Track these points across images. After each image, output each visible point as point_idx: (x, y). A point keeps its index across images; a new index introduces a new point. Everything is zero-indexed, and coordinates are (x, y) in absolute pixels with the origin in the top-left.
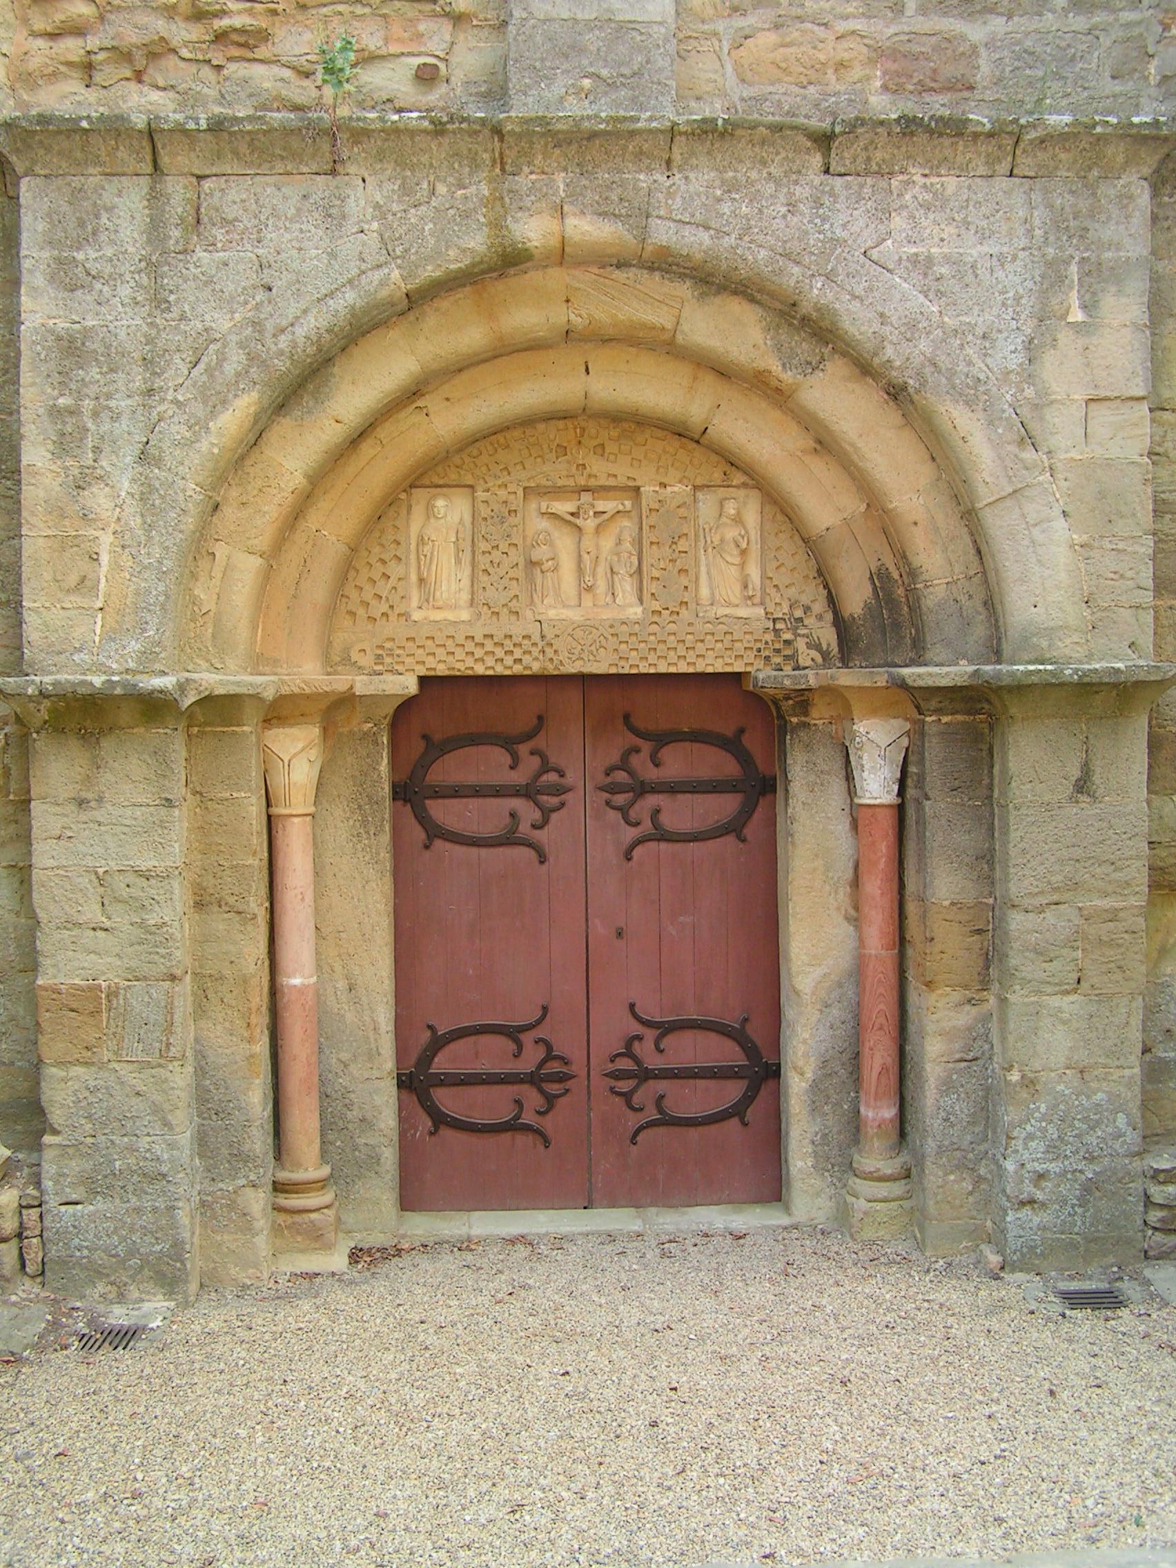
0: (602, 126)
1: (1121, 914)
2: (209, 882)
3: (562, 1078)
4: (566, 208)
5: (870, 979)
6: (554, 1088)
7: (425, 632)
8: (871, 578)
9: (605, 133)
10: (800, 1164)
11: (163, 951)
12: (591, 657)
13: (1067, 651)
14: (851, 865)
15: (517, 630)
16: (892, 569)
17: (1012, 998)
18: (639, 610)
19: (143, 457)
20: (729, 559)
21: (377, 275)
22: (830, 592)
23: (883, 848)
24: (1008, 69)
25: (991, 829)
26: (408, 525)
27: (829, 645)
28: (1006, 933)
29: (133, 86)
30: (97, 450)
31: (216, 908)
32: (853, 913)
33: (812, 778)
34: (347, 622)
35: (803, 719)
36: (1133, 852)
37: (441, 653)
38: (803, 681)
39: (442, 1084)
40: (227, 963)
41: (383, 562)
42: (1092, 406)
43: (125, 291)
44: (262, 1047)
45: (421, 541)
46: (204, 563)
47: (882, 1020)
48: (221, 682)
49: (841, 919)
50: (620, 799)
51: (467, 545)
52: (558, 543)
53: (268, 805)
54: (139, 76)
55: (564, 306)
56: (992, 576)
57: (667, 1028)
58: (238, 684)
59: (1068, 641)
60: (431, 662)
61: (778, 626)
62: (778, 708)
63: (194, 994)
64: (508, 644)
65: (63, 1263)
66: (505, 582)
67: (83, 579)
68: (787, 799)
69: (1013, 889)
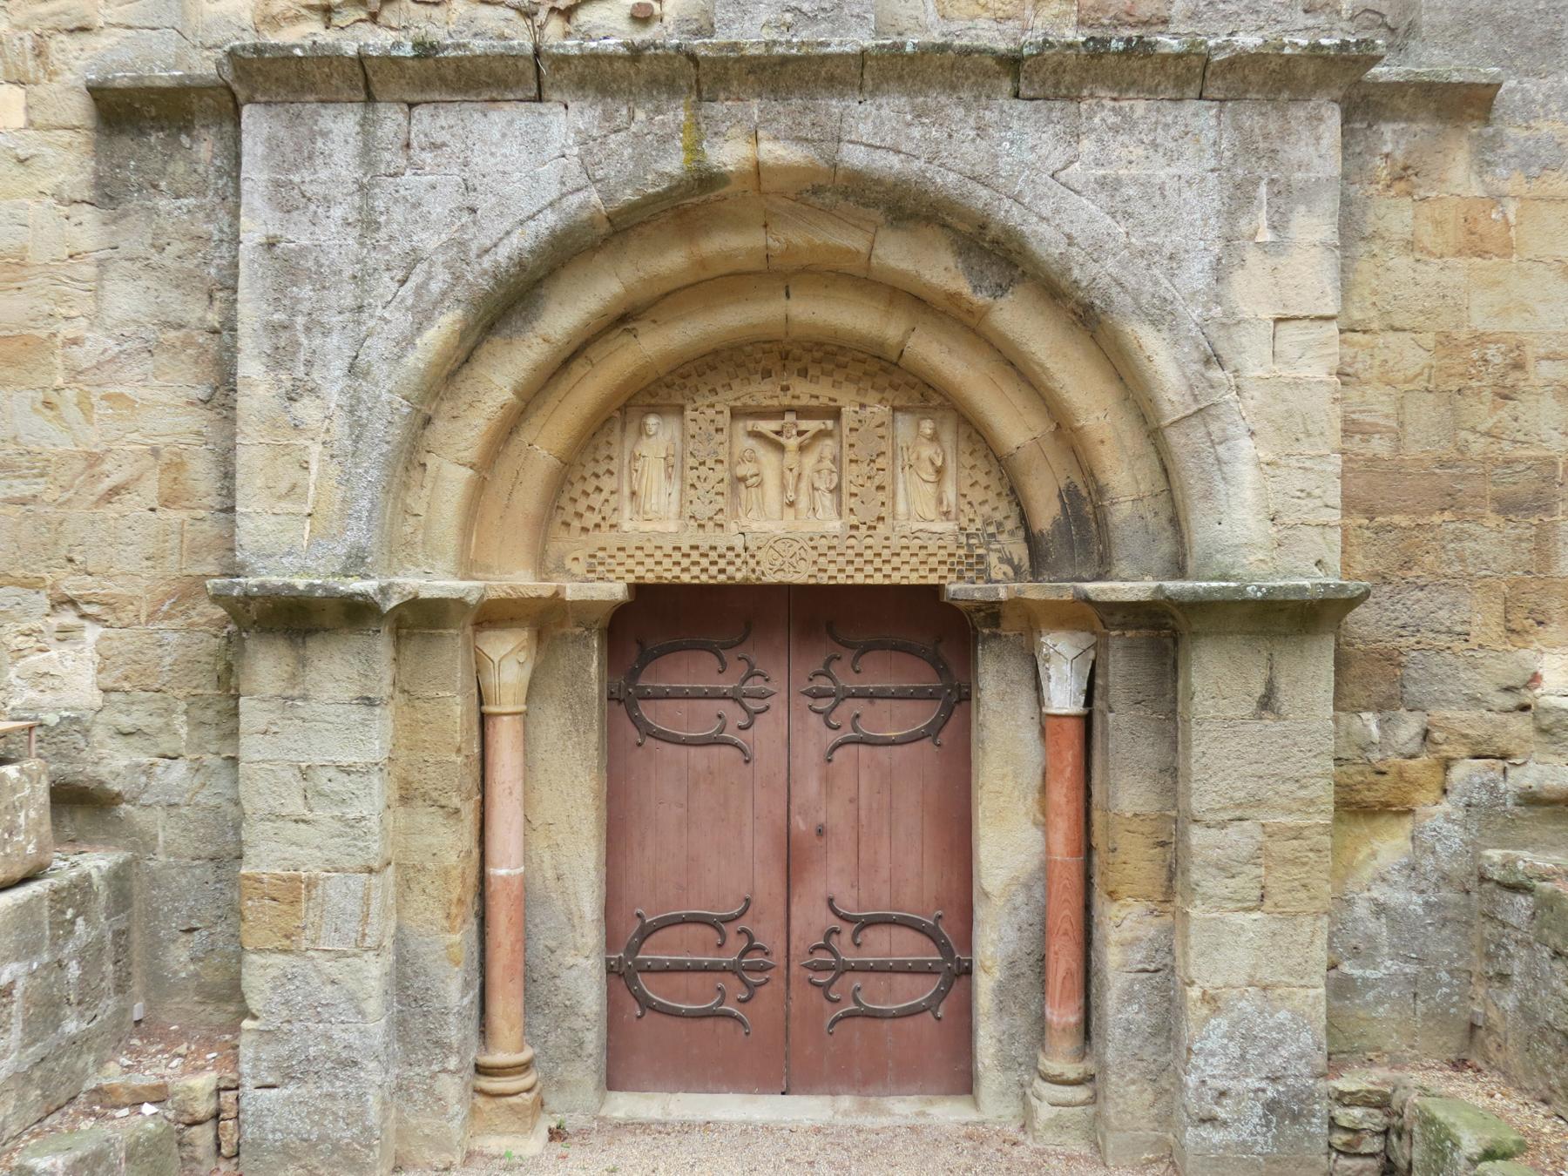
0: (794, 51)
1: (1306, 833)
2: (415, 776)
3: (763, 969)
4: (761, 133)
6: (754, 978)
8: (1060, 496)
9: (796, 59)
11: (361, 844)
13: (1253, 569)
14: (1039, 771)
16: (1081, 486)
17: (1193, 913)
19: (352, 370)
20: (925, 477)
21: (575, 200)
23: (1070, 756)
25: (1175, 743)
28: (1188, 848)
29: (367, 26)
30: (309, 363)
31: (420, 803)
32: (1040, 817)
34: (563, 533)
36: (1319, 770)
37: (649, 562)
39: (649, 970)
41: (597, 476)
42: (1281, 326)
43: (337, 212)
44: (462, 937)
46: (416, 474)
47: (1067, 926)
49: (1029, 824)
50: (824, 704)
51: (676, 461)
53: (481, 703)
54: (374, 17)
55: (763, 231)
56: (1178, 495)
59: (1252, 558)
60: (640, 571)
61: (972, 541)
63: (397, 884)
64: (713, 555)
65: (256, 1145)
66: (711, 496)
67: (294, 487)
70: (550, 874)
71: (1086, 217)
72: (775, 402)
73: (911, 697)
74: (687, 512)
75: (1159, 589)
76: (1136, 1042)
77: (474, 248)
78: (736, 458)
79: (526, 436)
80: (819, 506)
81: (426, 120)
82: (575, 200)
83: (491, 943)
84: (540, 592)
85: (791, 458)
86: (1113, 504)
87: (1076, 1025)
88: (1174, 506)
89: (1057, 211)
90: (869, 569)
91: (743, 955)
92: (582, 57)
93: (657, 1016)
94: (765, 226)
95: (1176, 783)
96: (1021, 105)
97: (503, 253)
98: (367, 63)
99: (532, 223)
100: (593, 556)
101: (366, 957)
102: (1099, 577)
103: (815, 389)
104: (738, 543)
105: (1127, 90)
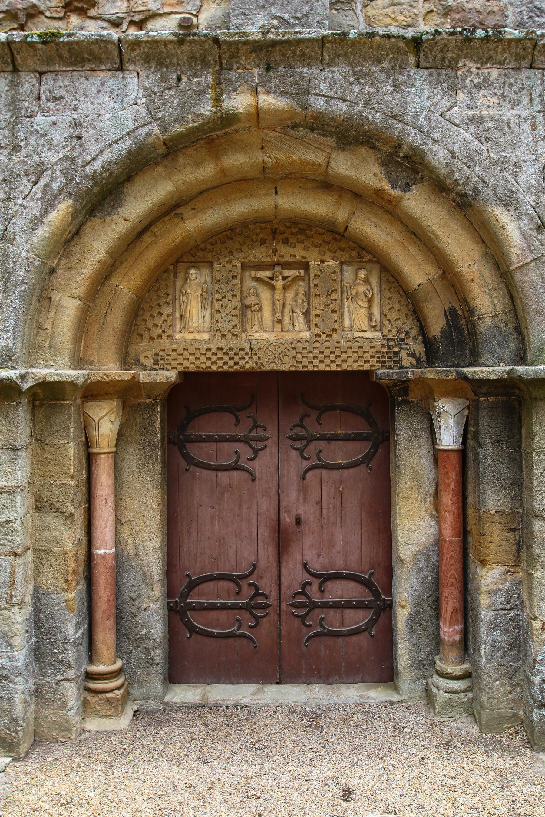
0: (280, 37)
3: (265, 607)
4: (260, 89)
5: (445, 555)
7: (183, 346)
8: (445, 315)
10: (403, 664)
11: (9, 538)
12: (280, 361)
15: (236, 344)
16: (457, 309)
17: (536, 574)
18: (308, 334)
20: (361, 304)
22: (421, 324)
24: (525, 17)
26: (175, 284)
27: (420, 354)
28: (532, 533)
32: (434, 512)
33: (410, 432)
34: (138, 339)
35: (405, 398)
37: (192, 358)
38: (405, 375)
39: (194, 609)
40: (55, 544)
44: (73, 595)
45: (181, 292)
47: (453, 580)
48: (51, 375)
50: (299, 444)
52: (262, 295)
55: (261, 151)
56: (520, 312)
57: (326, 578)
58: (60, 375)
60: (186, 364)
61: (391, 343)
62: (390, 392)
63: (34, 562)
64: (231, 354)
66: (230, 317)
68: (395, 446)
69: (536, 505)
70: (132, 552)
71: (462, 140)
72: (269, 259)
73: (354, 439)
74: (215, 327)
75: (510, 372)
76: (499, 654)
77: (80, 160)
78: (245, 294)
79: (114, 281)
80: (296, 323)
81: (51, 83)
82: (143, 131)
83: (95, 597)
84: (123, 377)
85: (279, 294)
86: (479, 319)
87: (460, 641)
88: (517, 320)
89: (444, 136)
90: (327, 361)
91: (252, 599)
92: (147, 42)
93: (200, 637)
94: (262, 148)
95: (522, 491)
96: (420, 72)
97: (98, 165)
98: (13, 46)
99: (116, 146)
100: (158, 355)
101: (13, 610)
102: (470, 365)
103: (293, 251)
104: (247, 346)
105: (486, 63)
